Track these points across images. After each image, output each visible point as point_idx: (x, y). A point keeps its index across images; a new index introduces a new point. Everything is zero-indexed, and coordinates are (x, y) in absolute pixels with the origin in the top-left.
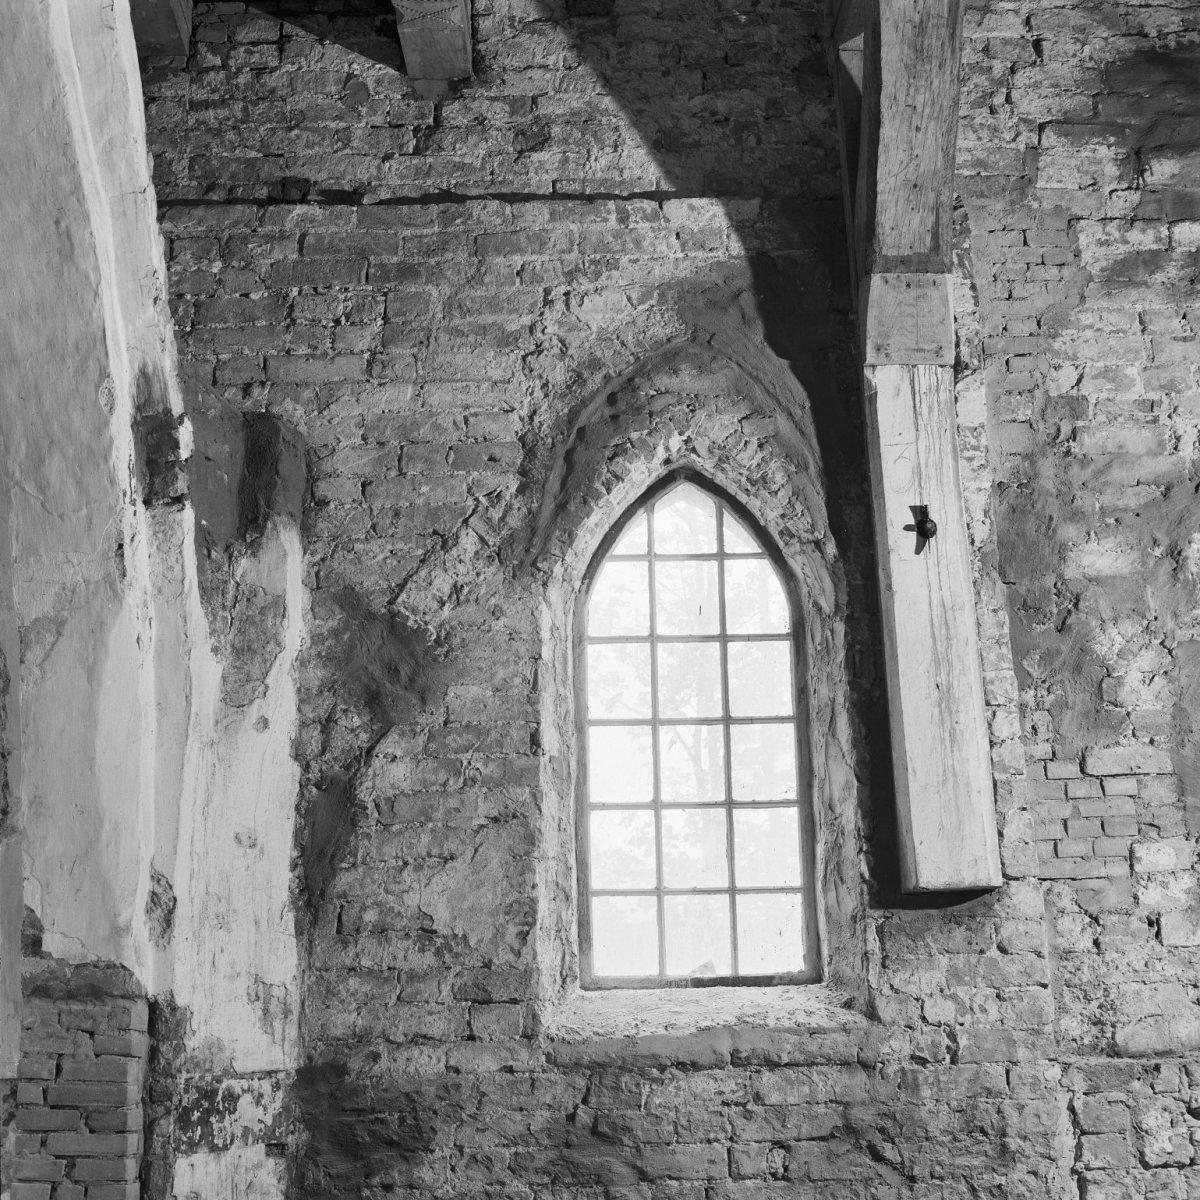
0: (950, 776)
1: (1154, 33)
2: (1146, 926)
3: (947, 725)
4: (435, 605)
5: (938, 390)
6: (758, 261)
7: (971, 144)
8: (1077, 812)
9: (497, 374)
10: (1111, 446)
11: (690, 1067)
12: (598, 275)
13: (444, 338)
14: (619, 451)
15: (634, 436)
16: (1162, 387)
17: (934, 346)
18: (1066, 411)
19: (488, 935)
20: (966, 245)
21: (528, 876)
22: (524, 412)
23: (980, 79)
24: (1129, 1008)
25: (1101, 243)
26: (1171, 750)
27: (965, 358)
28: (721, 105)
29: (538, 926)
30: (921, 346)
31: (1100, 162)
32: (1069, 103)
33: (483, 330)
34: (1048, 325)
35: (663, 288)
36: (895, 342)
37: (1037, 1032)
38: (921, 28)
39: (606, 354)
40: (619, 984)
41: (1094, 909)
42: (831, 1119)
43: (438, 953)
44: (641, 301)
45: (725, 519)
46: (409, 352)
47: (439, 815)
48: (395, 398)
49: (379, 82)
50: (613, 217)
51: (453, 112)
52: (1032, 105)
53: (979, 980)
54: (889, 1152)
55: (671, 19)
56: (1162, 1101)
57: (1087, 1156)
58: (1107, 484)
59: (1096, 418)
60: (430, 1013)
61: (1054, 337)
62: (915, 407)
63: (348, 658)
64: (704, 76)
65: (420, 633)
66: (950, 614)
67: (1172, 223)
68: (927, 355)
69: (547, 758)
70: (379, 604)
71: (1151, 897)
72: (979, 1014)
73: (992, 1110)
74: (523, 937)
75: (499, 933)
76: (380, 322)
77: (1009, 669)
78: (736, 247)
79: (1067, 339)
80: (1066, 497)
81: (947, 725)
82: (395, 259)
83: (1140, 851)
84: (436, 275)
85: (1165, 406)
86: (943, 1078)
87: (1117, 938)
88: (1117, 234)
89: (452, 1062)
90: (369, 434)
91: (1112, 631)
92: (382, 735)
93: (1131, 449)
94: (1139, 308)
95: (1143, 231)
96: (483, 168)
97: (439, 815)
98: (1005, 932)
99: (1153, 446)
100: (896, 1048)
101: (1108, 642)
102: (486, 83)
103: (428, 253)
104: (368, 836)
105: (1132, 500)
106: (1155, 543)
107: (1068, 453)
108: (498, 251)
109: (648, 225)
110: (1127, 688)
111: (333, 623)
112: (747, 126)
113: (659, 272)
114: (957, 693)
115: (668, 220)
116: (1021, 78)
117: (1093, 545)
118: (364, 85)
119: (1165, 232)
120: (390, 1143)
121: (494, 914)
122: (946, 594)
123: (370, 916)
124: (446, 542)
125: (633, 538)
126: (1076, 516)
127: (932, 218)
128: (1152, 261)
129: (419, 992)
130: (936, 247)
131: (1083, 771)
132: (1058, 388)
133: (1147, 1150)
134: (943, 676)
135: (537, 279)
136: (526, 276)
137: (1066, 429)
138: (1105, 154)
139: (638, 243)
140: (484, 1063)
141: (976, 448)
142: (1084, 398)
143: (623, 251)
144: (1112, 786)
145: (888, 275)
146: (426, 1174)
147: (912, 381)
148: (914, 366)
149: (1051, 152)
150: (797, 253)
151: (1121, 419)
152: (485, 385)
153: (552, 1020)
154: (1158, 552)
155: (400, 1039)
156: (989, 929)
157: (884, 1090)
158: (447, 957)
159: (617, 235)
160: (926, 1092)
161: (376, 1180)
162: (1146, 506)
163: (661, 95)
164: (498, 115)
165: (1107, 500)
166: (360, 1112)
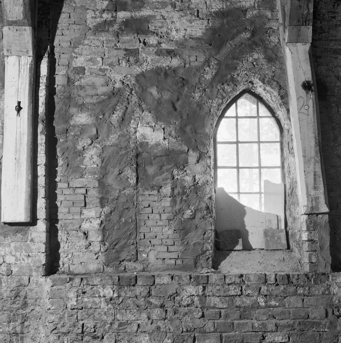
2: (83, 235)
3: (17, 171)
16: (109, 64)
17: (26, 50)
30: (22, 50)
36: (13, 48)
42: (306, 273)
53: (23, 250)
61: (76, 47)
62: (19, 69)
66: (22, 136)
68: (24, 53)
72: (22, 261)
77: (43, 154)
79: (80, 49)
81: (17, 171)
88: (99, 15)
95: (108, 14)
98: (33, 236)
110: (86, 160)
134: (18, 156)
145: (10, 27)
147: (19, 61)
148: (20, 56)
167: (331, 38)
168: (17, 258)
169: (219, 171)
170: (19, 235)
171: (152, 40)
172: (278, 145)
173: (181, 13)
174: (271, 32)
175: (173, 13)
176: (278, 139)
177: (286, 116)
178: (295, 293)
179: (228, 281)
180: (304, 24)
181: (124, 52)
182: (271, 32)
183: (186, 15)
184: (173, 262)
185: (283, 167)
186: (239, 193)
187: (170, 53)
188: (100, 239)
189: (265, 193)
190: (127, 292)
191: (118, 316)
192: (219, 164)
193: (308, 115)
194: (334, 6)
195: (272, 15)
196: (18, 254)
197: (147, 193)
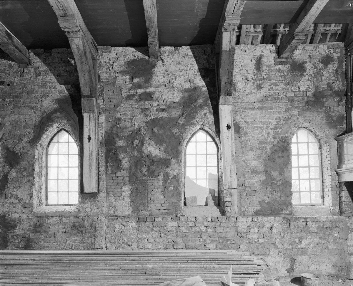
0: (90, 176)
1: (137, 56)
4: (20, 150)
5: (93, 117)
6: (71, 95)
7: (106, 76)
8: (114, 181)
9: (30, 113)
10: (124, 126)
11: (53, 217)
12: (46, 97)
13: (22, 108)
14: (48, 126)
15: (50, 123)
18: (118, 120)
19: (26, 198)
20: (103, 93)
21: (32, 190)
22: (35, 120)
23: (108, 64)
24: (119, 210)
25: (125, 93)
26: (129, 173)
27: (101, 112)
28: (67, 69)
29: (33, 197)
31: (126, 79)
32: (122, 69)
33: (28, 106)
34: (117, 106)
35: (56, 100)
36: (86, 109)
37: (102, 213)
38: (81, 57)
39: (46, 110)
40: (51, 205)
41: (115, 196)
42: (72, 225)
43: (19, 200)
44: (53, 102)
45: (207, 137)
46: (17, 110)
47: (19, 181)
48: (14, 117)
49: (14, 65)
50: (48, 88)
51: (25, 69)
52: (116, 69)
54: (80, 229)
55: (60, 54)
56: (118, 223)
57: (107, 231)
58: (123, 132)
59: (122, 121)
60: (17, 209)
63: (7, 157)
64: (65, 64)
65: (17, 154)
67: (137, 89)
69: (36, 172)
70: (12, 150)
71: (123, 194)
73: (95, 224)
74: (31, 198)
75: (27, 198)
76: (13, 105)
78: (67, 93)
80: (117, 134)
82: (15, 95)
83: (123, 188)
84: (21, 98)
85: (133, 119)
86: (88, 219)
87: (118, 200)
88: (128, 91)
89: (20, 216)
90: (11, 122)
91: (122, 155)
92: (11, 169)
93: (127, 126)
94: (131, 103)
95: (132, 91)
96: (30, 79)
97: (19, 181)
98: (98, 199)
99: (131, 126)
100: (82, 215)
101: (121, 156)
102: (30, 65)
103: (20, 94)
104: (9, 183)
105: (126, 134)
106: (129, 141)
107: (118, 127)
108: (31, 93)
109: (54, 89)
111: (4, 152)
112: (71, 72)
113: (56, 97)
114: (92, 164)
115: (57, 89)
116: (115, 64)
117: (120, 141)
118: (12, 65)
119: (136, 91)
120: (11, 227)
121: (27, 195)
122: (92, 149)
123: (9, 195)
124: (22, 140)
125: (193, 139)
126: (118, 137)
127: (90, 89)
128: (133, 96)
129: (16, 206)
130: (91, 94)
131: (115, 176)
132: (117, 116)
133: (115, 230)
135: (37, 98)
136: (35, 98)
137: (118, 123)
138: (127, 78)
139: (52, 92)
140: (24, 216)
141: (101, 126)
142: (121, 118)
143: (50, 94)
144: (120, 178)
146: (16, 231)
149: (119, 77)
150: (76, 94)
151: (126, 122)
152: (28, 115)
153: (35, 210)
154: (130, 143)
155: (13, 212)
156: (96, 198)
157: (80, 221)
158: (20, 201)
159: (49, 91)
160: (86, 221)
161: (9, 232)
162: (129, 135)
163: (58, 67)
164: (32, 70)
165: (123, 134)
166: (7, 222)
167: (243, 101)
168: (91, 209)
169: (187, 168)
170: (92, 199)
171: (155, 104)
172: (216, 156)
173: (168, 90)
174: (213, 99)
175: (164, 90)
176: (216, 153)
177: (219, 141)
178: (220, 226)
179: (189, 220)
180: (229, 95)
181: (140, 110)
182: (213, 99)
183: (171, 91)
184: (164, 211)
185: (218, 167)
186: (196, 179)
187: (163, 110)
188: (130, 200)
189: (209, 179)
190: (142, 224)
191: (138, 236)
192: (187, 165)
193: (228, 141)
194: (246, 84)
195: (214, 90)
196: (92, 207)
197: (151, 179)
